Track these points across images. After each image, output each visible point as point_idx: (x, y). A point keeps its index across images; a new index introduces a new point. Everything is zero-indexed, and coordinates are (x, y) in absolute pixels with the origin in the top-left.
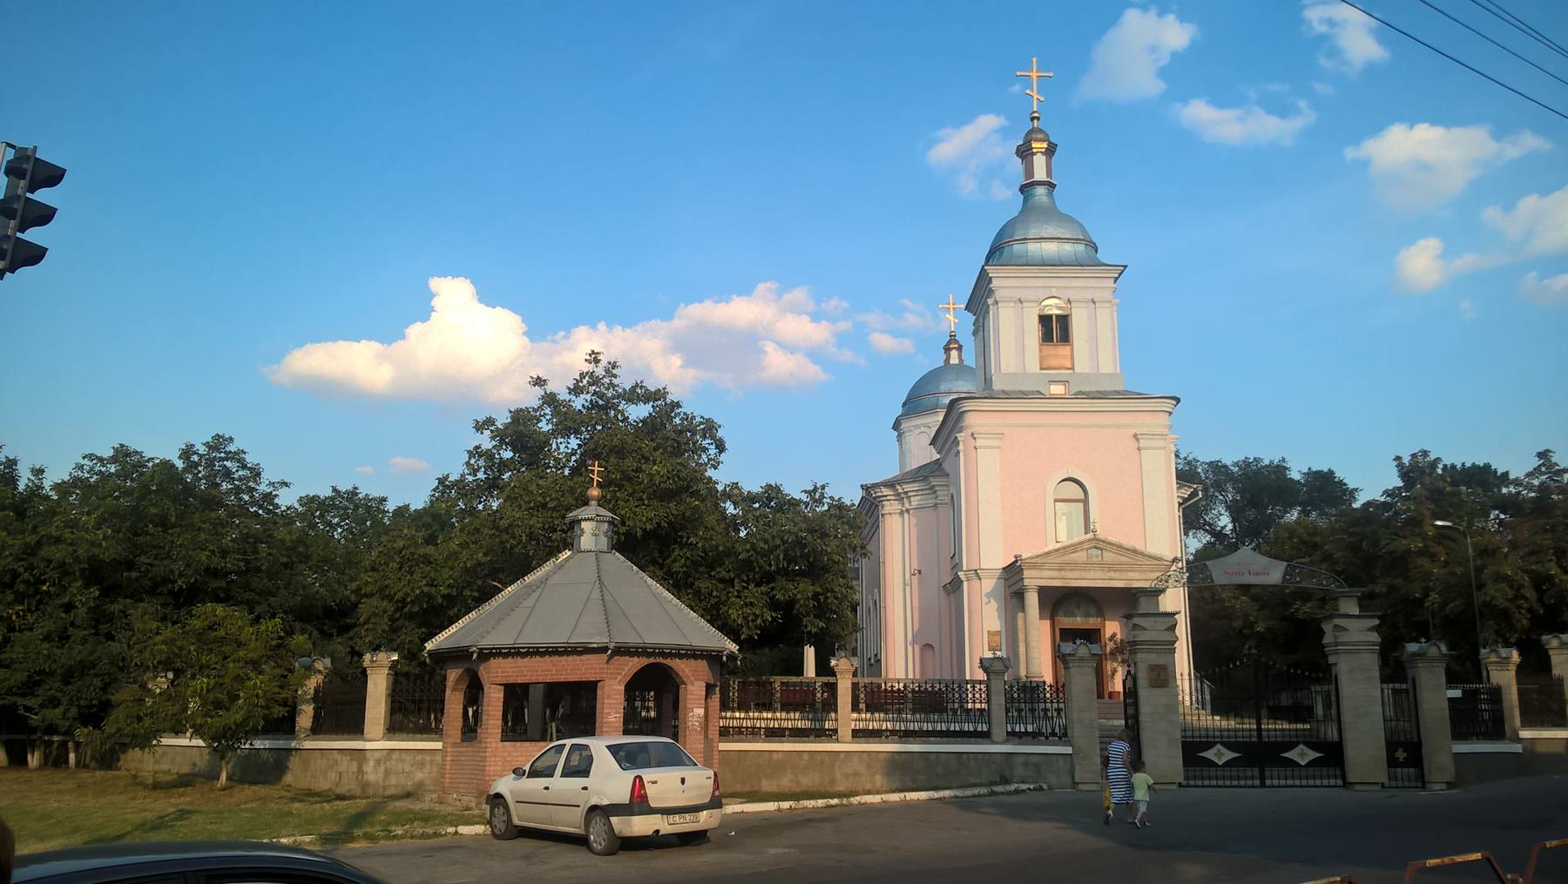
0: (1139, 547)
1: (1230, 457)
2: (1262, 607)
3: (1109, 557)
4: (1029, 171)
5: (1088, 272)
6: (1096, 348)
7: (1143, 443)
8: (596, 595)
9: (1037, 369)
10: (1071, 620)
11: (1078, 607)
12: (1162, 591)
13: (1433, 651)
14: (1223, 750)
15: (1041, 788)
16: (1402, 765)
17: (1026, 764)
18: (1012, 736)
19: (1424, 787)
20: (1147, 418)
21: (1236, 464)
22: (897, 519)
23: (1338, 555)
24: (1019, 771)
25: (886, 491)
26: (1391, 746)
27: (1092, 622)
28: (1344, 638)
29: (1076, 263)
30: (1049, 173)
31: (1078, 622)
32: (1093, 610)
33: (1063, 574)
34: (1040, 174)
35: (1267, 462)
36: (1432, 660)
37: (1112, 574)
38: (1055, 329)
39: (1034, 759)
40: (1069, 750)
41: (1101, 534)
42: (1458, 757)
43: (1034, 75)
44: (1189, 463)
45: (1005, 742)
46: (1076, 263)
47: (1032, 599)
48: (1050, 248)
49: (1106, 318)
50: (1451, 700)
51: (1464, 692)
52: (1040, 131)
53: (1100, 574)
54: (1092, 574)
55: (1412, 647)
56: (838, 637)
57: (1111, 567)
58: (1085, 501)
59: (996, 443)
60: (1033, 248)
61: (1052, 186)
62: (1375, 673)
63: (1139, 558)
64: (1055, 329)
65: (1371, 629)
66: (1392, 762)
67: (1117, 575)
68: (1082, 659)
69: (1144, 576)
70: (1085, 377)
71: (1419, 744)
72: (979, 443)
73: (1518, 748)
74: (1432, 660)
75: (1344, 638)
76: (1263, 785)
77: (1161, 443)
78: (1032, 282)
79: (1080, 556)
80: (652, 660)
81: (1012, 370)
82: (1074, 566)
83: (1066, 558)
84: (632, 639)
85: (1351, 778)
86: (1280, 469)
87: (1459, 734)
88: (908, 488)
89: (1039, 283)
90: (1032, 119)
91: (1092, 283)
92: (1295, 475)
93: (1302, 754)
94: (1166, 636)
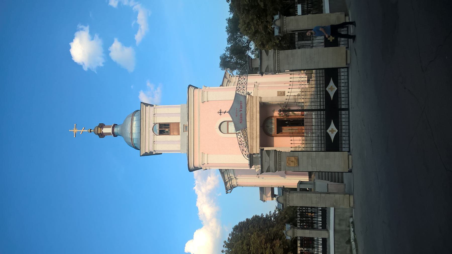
1: (226, 36)
2: (271, 40)
4: (109, 134)
5: (143, 117)
6: (170, 114)
7: (205, 100)
9: (179, 136)
10: (273, 129)
11: (268, 127)
13: (278, 23)
14: (330, 129)
15: (353, 223)
17: (339, 224)
18: (325, 226)
20: (196, 98)
21: (228, 34)
22: (238, 181)
23: (251, 17)
24: (344, 227)
25: (228, 185)
27: (274, 121)
29: (140, 120)
30: (109, 127)
31: (274, 127)
32: (270, 121)
33: (255, 137)
34: (109, 130)
35: (227, 25)
36: (282, 23)
37: (255, 118)
38: (164, 129)
39: (337, 221)
40: (332, 210)
42: (332, 11)
43: (75, 131)
44: (227, 50)
45: (328, 231)
46: (140, 120)
48: (135, 130)
49: (160, 110)
50: (303, 13)
51: (299, 3)
52: (94, 130)
53: (255, 123)
54: (255, 126)
55: (277, 33)
59: (206, 155)
60: (134, 136)
61: (115, 125)
62: (289, 52)
64: (164, 129)
65: (267, 53)
67: (255, 116)
68: (285, 200)
69: (255, 106)
70: (182, 118)
72: (206, 162)
74: (282, 23)
76: (348, 109)
77: (205, 93)
78: (147, 137)
81: (179, 146)
86: (229, 21)
87: (320, 10)
88: (226, 178)
89: (147, 135)
90: (91, 132)
91: (147, 115)
92: (231, 16)
93: (332, 89)
94: (272, 155)
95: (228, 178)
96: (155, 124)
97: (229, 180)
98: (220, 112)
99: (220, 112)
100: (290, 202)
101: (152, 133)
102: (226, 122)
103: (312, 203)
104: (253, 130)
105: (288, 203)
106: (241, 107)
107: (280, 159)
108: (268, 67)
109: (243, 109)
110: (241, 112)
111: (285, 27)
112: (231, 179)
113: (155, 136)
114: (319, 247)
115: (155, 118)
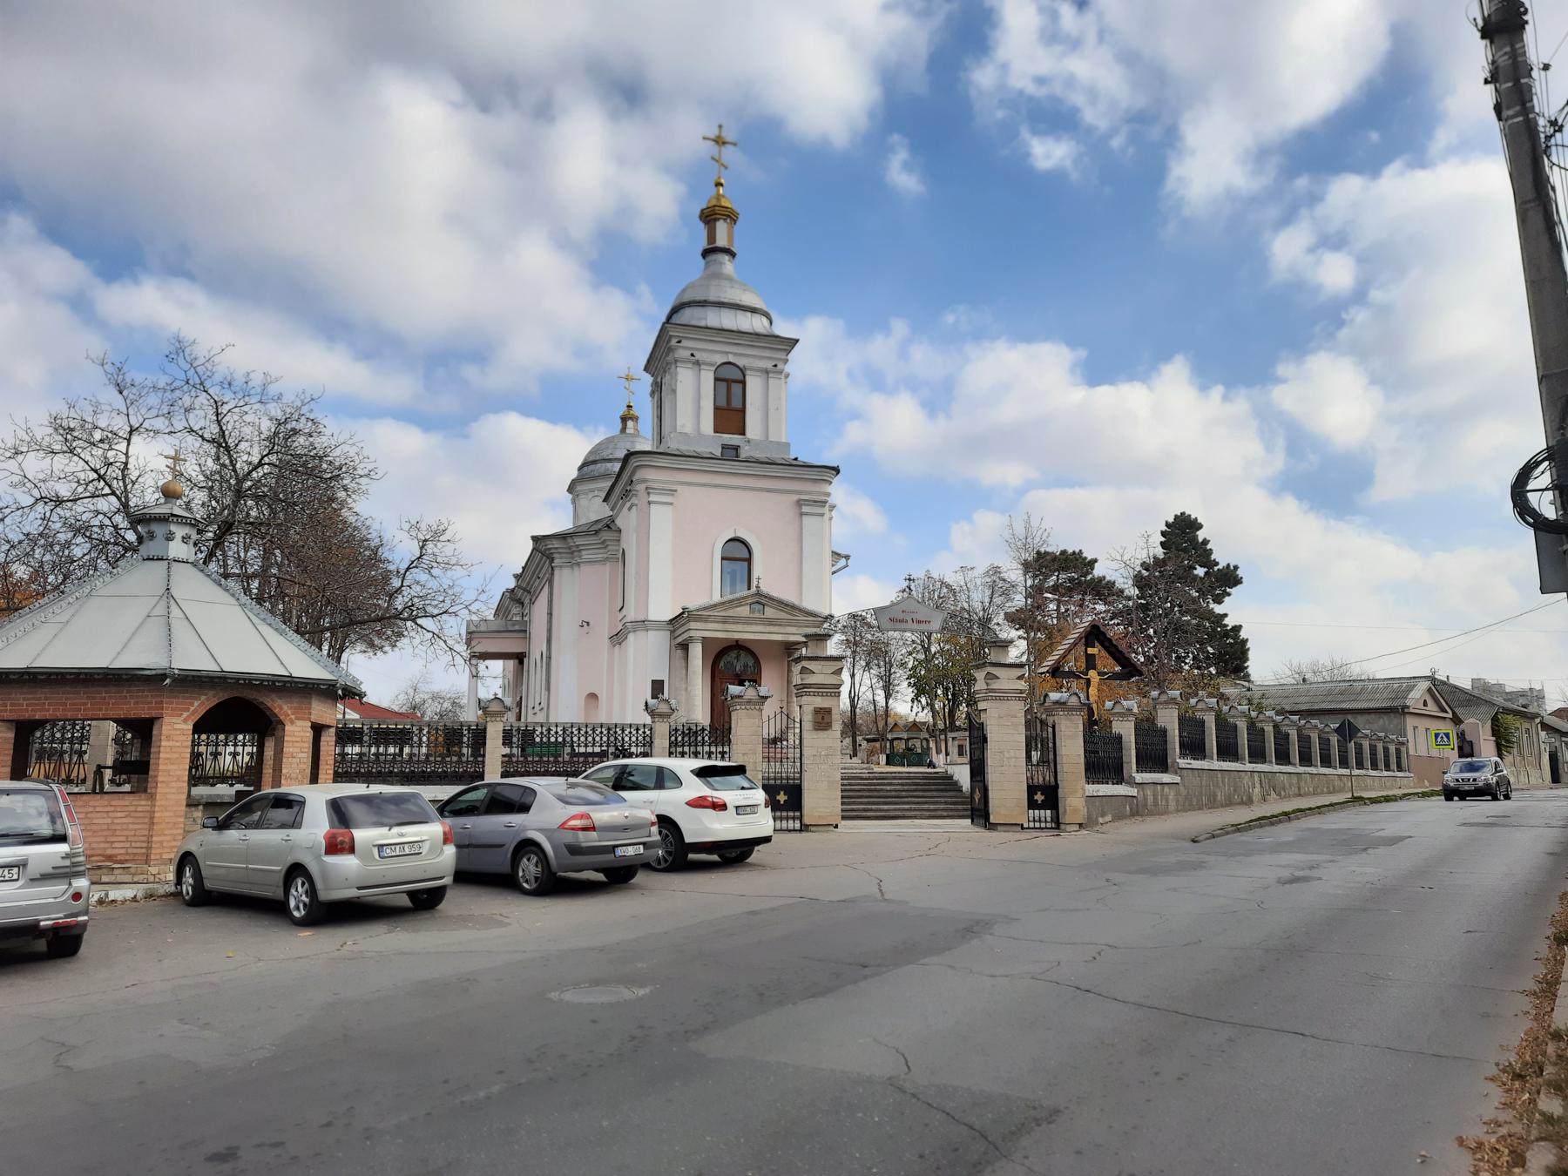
0: (796, 603)
3: (770, 612)
8: (161, 610)
12: (1311, 250)
16: (1040, 807)
19: (1058, 828)
25: (556, 544)
26: (1032, 790)
28: (995, 685)
30: (730, 238)
36: (1072, 709)
37: (772, 629)
41: (765, 589)
47: (696, 651)
56: (282, 437)
57: (771, 622)
58: (749, 560)
63: (797, 613)
66: (1032, 804)
71: (1057, 786)
72: (653, 498)
73: (1133, 792)
74: (1072, 709)
75: (995, 685)
79: (744, 611)
80: (235, 694)
82: (737, 620)
83: (730, 613)
84: (204, 664)
85: (806, 821)
94: (832, 680)
96: (743, 371)
101: (719, 359)
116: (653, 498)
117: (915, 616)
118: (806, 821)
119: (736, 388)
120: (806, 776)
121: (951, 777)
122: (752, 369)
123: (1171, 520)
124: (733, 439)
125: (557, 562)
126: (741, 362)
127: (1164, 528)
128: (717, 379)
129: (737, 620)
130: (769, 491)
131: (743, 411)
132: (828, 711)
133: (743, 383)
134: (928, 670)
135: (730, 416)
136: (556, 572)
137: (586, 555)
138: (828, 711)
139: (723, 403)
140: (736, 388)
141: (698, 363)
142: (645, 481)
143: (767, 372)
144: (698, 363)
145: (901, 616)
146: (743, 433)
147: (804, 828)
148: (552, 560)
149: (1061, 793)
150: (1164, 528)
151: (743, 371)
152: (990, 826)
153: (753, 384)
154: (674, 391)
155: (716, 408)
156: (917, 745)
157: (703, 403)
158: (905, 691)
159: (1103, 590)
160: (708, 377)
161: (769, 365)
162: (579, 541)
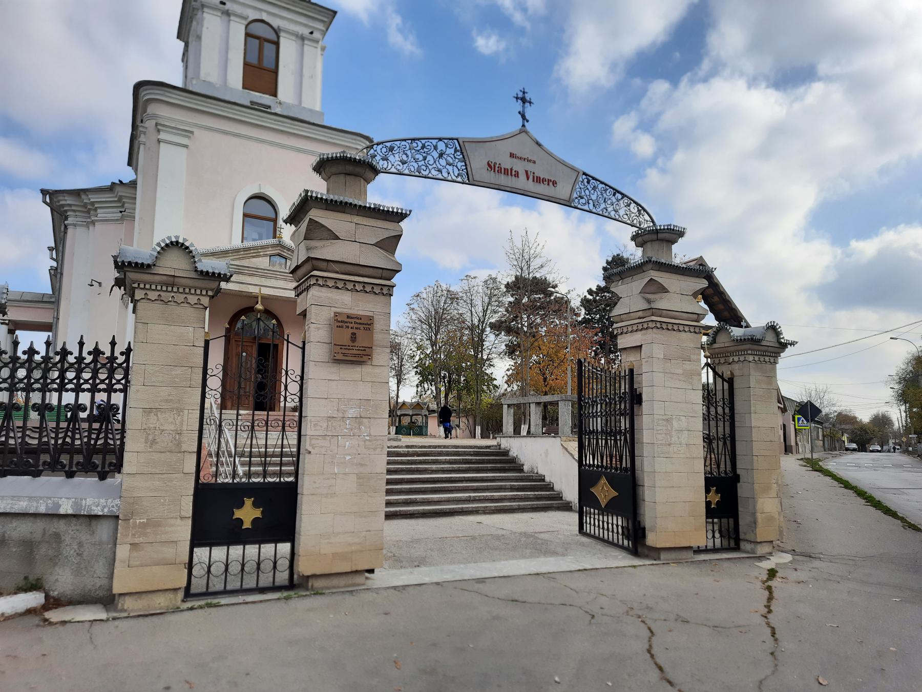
25: (69, 200)
28: (663, 303)
68: (171, 283)
71: (737, 478)
72: (162, 136)
79: (263, 262)
94: (376, 259)
95: (93, 203)
96: (277, 32)
97: (85, 205)
98: (524, 100)
99: (524, 100)
100: (158, 306)
101: (253, 15)
102: (274, 216)
103: (148, 411)
104: (261, 276)
105: (153, 295)
106: (538, 180)
107: (365, 289)
108: (663, 290)
109: (531, 186)
110: (522, 176)
111: (757, 358)
112: (88, 212)
113: (246, 22)
114: (55, 402)
115: (294, 38)
116: (162, 136)
117: (530, 167)
118: (304, 567)
119: (269, 49)
120: (308, 464)
121: (506, 453)
122: (287, 32)
123: (610, 259)
124: (266, 99)
125: (70, 221)
126: (275, 22)
127: (605, 265)
128: (248, 35)
129: (254, 272)
130: (299, 150)
131: (276, 72)
132: (367, 324)
133: (277, 44)
134: (435, 361)
135: (261, 74)
136: (70, 231)
137: (102, 214)
138: (367, 324)
139: (254, 60)
140: (269, 49)
141: (227, 13)
142: (154, 116)
143: (302, 38)
144: (227, 13)
145: (507, 163)
146: (275, 94)
147: (296, 584)
148: (66, 218)
149: (742, 490)
150: (605, 265)
151: (277, 32)
152: (654, 553)
153: (288, 47)
154: (199, 37)
155: (246, 64)
156: (419, 420)
157: (231, 55)
158: (412, 378)
159: (562, 304)
160: (238, 32)
161: (306, 32)
162: (94, 198)
